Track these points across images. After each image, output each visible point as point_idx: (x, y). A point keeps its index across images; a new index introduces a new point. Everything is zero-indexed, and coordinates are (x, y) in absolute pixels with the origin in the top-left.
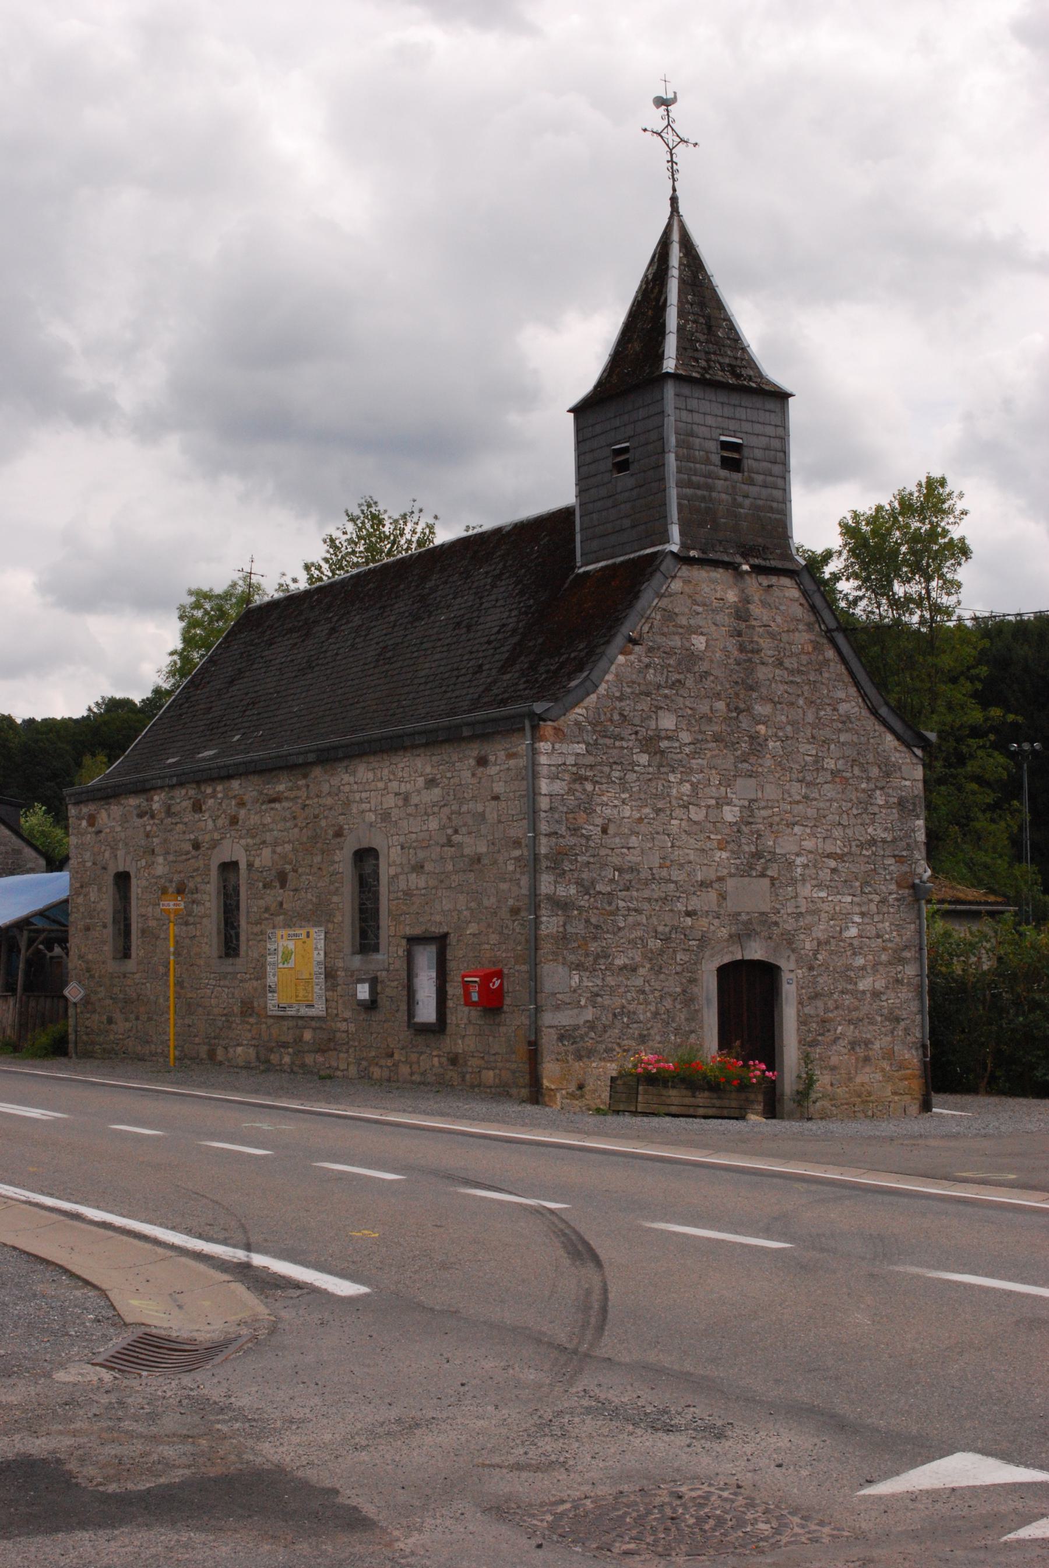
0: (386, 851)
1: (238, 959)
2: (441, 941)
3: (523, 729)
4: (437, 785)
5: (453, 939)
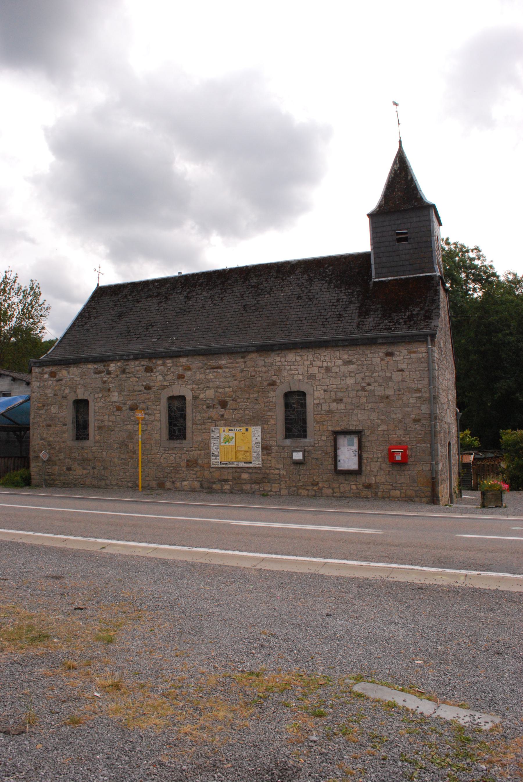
0: (312, 393)
2: (359, 433)
3: (427, 341)
4: (353, 364)
5: (367, 432)
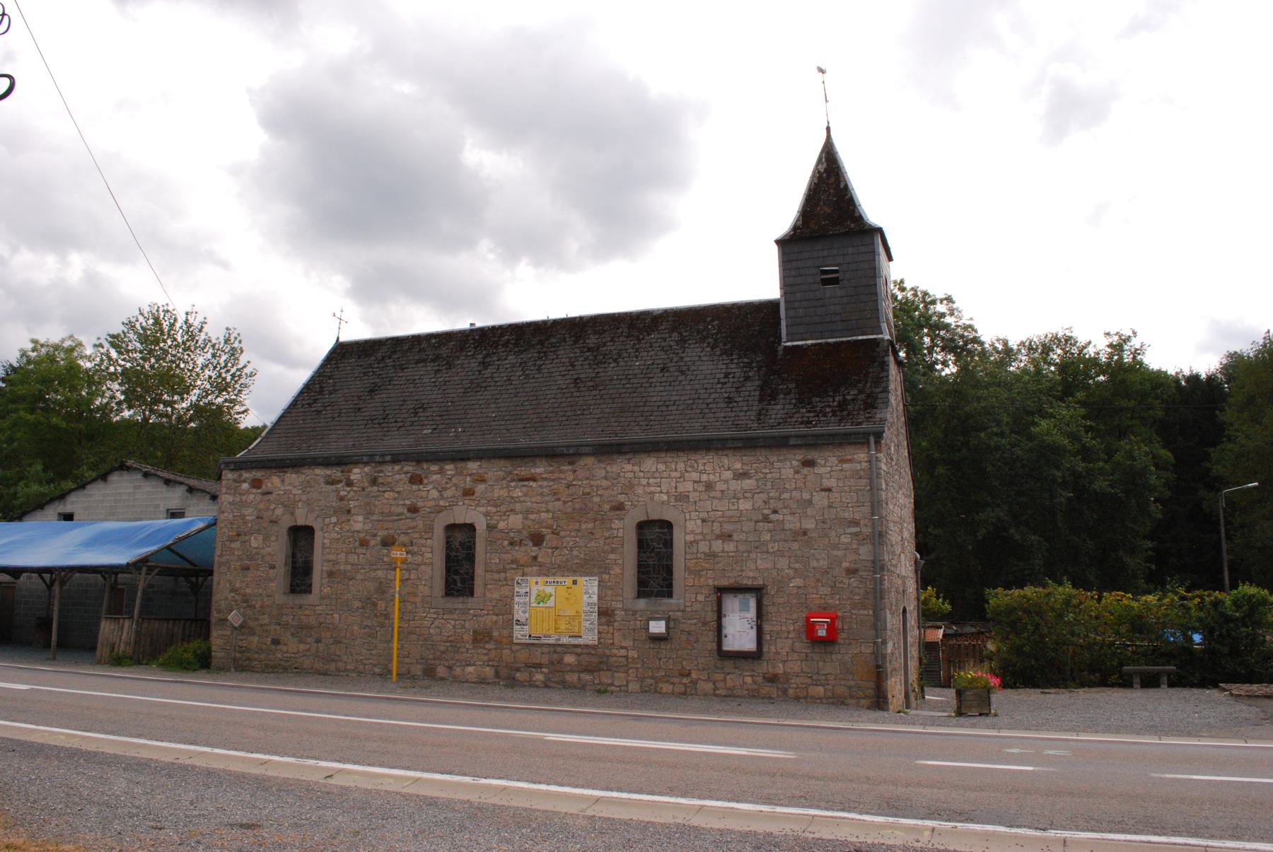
1: (470, 599)
2: (758, 591)
3: (868, 443)
4: (750, 478)
5: (771, 590)
